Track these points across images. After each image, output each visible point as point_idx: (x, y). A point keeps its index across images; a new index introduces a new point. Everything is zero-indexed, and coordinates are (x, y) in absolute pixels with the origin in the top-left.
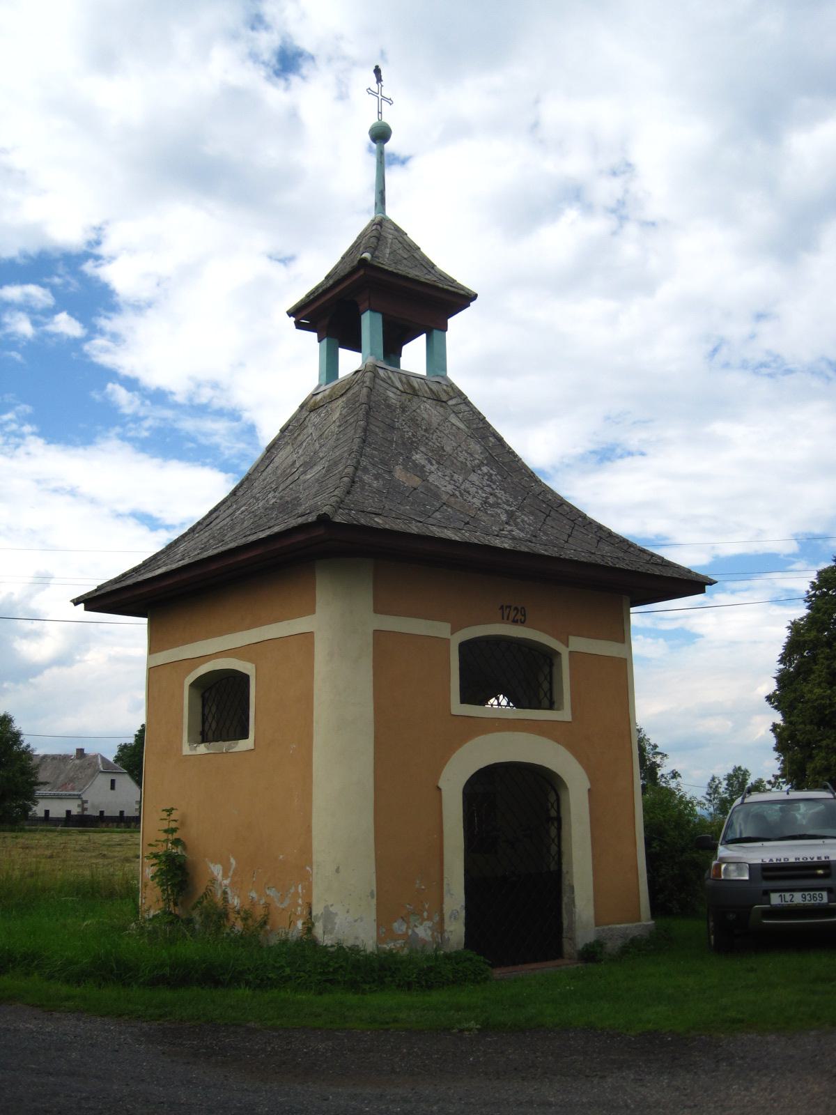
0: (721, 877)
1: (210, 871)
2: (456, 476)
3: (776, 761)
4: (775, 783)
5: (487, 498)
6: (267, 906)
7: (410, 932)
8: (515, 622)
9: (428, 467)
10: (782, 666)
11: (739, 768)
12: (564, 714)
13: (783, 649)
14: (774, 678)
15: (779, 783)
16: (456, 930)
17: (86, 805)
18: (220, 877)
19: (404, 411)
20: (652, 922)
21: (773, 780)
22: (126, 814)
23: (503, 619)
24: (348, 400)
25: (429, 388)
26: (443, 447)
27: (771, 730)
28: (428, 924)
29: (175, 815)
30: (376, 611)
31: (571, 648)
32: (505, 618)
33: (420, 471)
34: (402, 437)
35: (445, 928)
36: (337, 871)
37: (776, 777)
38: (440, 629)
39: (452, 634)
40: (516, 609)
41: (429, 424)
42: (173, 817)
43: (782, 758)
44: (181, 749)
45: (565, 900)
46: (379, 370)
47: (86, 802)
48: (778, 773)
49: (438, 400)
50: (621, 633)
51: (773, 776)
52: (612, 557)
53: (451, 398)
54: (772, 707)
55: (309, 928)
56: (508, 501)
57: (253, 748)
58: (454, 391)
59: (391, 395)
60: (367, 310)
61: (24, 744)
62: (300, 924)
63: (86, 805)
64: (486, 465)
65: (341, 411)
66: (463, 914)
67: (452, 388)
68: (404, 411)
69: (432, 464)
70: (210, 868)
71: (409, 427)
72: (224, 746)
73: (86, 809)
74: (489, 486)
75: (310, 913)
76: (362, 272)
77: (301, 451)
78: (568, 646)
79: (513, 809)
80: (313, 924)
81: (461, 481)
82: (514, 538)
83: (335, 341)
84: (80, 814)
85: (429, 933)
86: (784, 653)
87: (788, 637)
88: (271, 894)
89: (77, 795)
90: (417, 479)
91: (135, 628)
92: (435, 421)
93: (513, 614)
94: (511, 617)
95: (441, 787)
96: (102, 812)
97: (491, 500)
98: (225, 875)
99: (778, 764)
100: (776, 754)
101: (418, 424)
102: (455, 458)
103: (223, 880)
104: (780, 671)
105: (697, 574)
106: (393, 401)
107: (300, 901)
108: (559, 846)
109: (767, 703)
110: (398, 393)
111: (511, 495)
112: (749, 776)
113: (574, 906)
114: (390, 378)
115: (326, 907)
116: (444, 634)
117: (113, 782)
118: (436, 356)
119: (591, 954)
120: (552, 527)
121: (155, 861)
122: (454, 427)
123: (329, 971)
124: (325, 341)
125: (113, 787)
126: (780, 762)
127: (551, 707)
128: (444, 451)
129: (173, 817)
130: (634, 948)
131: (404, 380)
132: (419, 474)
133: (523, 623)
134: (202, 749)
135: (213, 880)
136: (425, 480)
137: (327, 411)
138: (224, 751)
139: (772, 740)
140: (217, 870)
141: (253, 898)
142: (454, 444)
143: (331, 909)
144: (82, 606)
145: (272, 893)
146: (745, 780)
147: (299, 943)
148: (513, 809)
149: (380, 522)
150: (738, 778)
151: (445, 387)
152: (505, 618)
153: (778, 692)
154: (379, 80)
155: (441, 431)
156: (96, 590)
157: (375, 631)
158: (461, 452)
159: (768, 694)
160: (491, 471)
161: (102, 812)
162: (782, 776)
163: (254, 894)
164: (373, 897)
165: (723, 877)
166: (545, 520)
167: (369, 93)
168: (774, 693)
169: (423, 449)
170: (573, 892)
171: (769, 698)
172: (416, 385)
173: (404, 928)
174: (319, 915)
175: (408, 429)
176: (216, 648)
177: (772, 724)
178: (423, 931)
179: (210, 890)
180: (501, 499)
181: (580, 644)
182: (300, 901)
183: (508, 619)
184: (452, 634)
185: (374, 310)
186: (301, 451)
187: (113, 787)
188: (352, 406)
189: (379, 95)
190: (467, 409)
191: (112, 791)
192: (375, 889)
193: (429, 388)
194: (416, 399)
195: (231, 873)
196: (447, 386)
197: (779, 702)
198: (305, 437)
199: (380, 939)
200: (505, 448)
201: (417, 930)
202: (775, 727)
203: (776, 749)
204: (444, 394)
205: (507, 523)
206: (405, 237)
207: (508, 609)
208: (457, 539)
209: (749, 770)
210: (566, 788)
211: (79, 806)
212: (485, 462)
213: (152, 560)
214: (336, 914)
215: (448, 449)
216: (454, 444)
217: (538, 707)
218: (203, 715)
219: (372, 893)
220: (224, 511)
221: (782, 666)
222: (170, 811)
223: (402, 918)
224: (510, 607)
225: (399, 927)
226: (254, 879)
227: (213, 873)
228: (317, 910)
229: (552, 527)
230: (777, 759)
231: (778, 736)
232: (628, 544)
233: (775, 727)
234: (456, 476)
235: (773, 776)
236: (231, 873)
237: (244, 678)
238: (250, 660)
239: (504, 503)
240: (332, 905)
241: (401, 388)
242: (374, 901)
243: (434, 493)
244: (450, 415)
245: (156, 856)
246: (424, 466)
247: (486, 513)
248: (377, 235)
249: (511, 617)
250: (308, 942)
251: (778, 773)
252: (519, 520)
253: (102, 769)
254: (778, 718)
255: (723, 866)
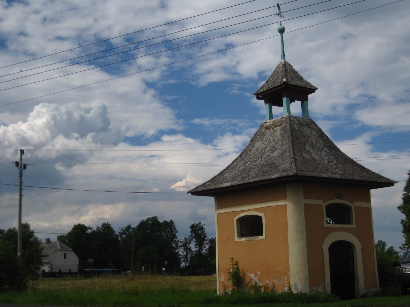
0: (403, 272)
1: (249, 276)
2: (318, 153)
3: (403, 238)
4: (403, 248)
5: (328, 160)
6: (273, 284)
7: (317, 289)
8: (339, 198)
9: (311, 151)
10: (405, 192)
11: (381, 241)
13: (406, 184)
14: (402, 198)
15: (405, 248)
16: (329, 289)
17: (53, 267)
18: (253, 278)
19: (300, 132)
20: (380, 289)
21: (402, 246)
22: (62, 271)
23: (336, 197)
24: (282, 128)
25: (305, 122)
26: (312, 143)
27: (400, 223)
28: (321, 287)
29: (234, 260)
30: (305, 198)
32: (337, 197)
33: (308, 152)
34: (301, 141)
35: (326, 288)
36: (298, 272)
37: (404, 245)
38: (320, 202)
39: (324, 203)
40: (340, 194)
41: (307, 135)
42: (233, 261)
43: (406, 236)
44: (234, 240)
45: (356, 281)
47: (52, 265)
48: (404, 243)
49: (309, 126)
50: (368, 199)
51: (402, 244)
52: (366, 177)
53: (311, 124)
54: (401, 212)
55: (290, 289)
56: (334, 160)
57: (265, 238)
58: (312, 122)
59: (295, 126)
60: (285, 97)
62: (286, 288)
63: (53, 267)
64: (325, 147)
65: (280, 132)
66: (330, 285)
67: (311, 120)
68: (300, 132)
69: (311, 150)
70: (249, 275)
71: (302, 137)
72: (253, 238)
74: (327, 155)
75: (290, 285)
76: (284, 86)
77: (266, 144)
78: (354, 205)
79: (342, 254)
80: (291, 288)
81: (320, 155)
82: (340, 174)
84: (50, 271)
85: (322, 290)
86: (406, 186)
87: (408, 178)
88: (275, 281)
89: (48, 262)
90: (309, 156)
92: (309, 133)
95: (323, 248)
96: (60, 270)
97: (329, 160)
98: (256, 277)
99: (404, 239)
100: (403, 234)
101: (304, 136)
102: (316, 146)
103: (255, 278)
104: (404, 195)
105: (391, 180)
106: (297, 128)
107: (286, 282)
108: (353, 265)
109: (398, 210)
110: (297, 125)
111: (334, 157)
112: (386, 245)
113: (359, 283)
114: (294, 120)
115: (295, 283)
116: (322, 203)
117: (65, 255)
118: (304, 108)
119: (365, 296)
120: (348, 168)
121: (229, 274)
122: (314, 135)
123: (301, 299)
125: (65, 257)
126: (405, 238)
127: (349, 223)
128: (313, 144)
129: (233, 261)
130: (375, 295)
132: (309, 154)
133: (342, 198)
134: (243, 239)
135: (251, 278)
136: (311, 156)
137: (273, 130)
138: (253, 239)
139: (401, 227)
140: (252, 276)
141: (267, 283)
142: (315, 141)
143: (296, 283)
144: (190, 194)
145: (275, 280)
146: (384, 247)
147: (288, 293)
148: (342, 254)
149: (308, 174)
150: (380, 246)
152: (337, 197)
153: (403, 205)
154: (279, 9)
155: (311, 137)
156: (196, 188)
157: (304, 204)
158: (317, 144)
159: (399, 206)
160: (327, 149)
161: (60, 270)
162: (406, 244)
163: (268, 281)
164: (308, 280)
165: (404, 273)
167: (277, 15)
168: (402, 205)
169: (307, 144)
170: (358, 279)
171: (399, 208)
173: (316, 288)
174: (293, 285)
175: (302, 138)
177: (401, 220)
178: (320, 289)
179: (250, 282)
180: (332, 159)
181: (357, 204)
182: (286, 282)
183: (338, 198)
184: (324, 203)
185: (287, 97)
186: (266, 144)
187: (65, 257)
188: (283, 129)
189: (280, 15)
190: (316, 127)
191: (65, 260)
192: (308, 277)
193: (305, 122)
194: (302, 127)
195: (258, 276)
196: (310, 120)
197: (404, 210)
198: (267, 139)
199: (310, 292)
200: (329, 140)
201: (319, 289)
202: (402, 222)
203: (403, 232)
205: (336, 168)
206: (292, 68)
208: (327, 177)
209: (386, 242)
210: (355, 248)
211: (49, 267)
212: (324, 146)
213: (214, 178)
214: (298, 284)
215: (314, 143)
216: (315, 141)
217: (346, 224)
218: (241, 228)
219: (308, 278)
220: (240, 163)
221: (405, 192)
222: (232, 259)
223: (315, 285)
225: (315, 288)
226: (268, 277)
227: (250, 276)
228: (292, 284)
229: (348, 168)
230: (404, 236)
231: (404, 226)
232: (369, 171)
233: (402, 222)
234: (318, 153)
235: (402, 244)
236: (258, 276)
237: (260, 218)
238: (262, 212)
240: (297, 282)
241: (298, 123)
242: (308, 281)
243: (314, 160)
244: (312, 131)
245: (230, 273)
246: (309, 151)
247: (330, 165)
248: (285, 70)
250: (290, 293)
251: (404, 243)
252: (339, 167)
253: (59, 248)
254: (403, 217)
255: (404, 269)
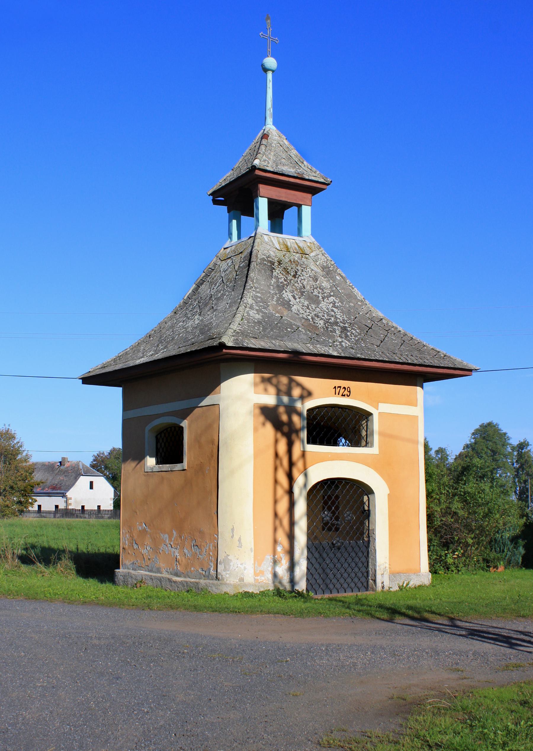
12: (374, 450)
31: (380, 411)
40: (344, 388)
46: (265, 236)
61: (24, 454)
73: (70, 504)
78: (378, 409)
83: (239, 212)
91: (115, 394)
93: (342, 391)
94: (341, 394)
101: (288, 272)
117: (91, 483)
124: (232, 212)
125: (91, 487)
131: (281, 241)
151: (309, 244)
164: (252, 552)
166: (367, 332)
172: (289, 244)
176: (159, 412)
181: (385, 408)
187: (91, 487)
191: (91, 490)
204: (308, 249)
207: (339, 388)
224: (340, 387)
239: (341, 322)
249: (341, 394)
